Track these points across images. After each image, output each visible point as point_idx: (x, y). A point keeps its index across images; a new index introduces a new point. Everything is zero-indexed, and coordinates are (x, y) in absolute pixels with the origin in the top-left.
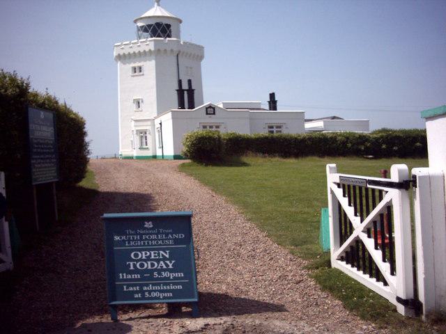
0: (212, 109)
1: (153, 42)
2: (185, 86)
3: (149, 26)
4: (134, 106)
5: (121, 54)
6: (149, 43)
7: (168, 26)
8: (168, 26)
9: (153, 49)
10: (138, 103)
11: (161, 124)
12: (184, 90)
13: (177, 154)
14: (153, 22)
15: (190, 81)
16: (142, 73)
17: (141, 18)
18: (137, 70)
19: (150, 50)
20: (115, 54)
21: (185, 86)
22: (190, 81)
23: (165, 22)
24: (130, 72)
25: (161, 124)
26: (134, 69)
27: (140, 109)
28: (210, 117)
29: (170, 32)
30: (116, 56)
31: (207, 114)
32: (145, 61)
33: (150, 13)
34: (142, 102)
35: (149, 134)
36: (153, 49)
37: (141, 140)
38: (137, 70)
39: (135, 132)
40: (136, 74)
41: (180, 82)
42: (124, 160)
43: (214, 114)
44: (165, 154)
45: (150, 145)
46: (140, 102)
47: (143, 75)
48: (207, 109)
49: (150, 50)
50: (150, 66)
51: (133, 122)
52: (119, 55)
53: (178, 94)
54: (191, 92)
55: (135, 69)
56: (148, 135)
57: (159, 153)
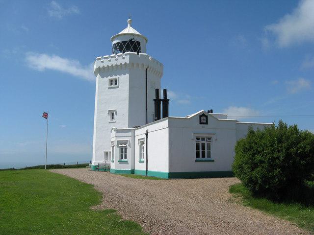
0: (205, 118)
1: (128, 56)
2: (162, 97)
3: (124, 42)
4: (109, 117)
5: (101, 67)
6: (124, 58)
7: (139, 43)
8: (139, 43)
9: (128, 62)
10: (112, 114)
11: (147, 134)
12: (161, 100)
13: (173, 171)
14: (127, 39)
15: (165, 91)
16: (117, 85)
17: (118, 36)
18: (114, 83)
19: (126, 63)
20: (95, 67)
21: (162, 97)
22: (165, 91)
23: (137, 39)
24: (108, 85)
25: (147, 134)
26: (111, 82)
27: (114, 121)
28: (203, 127)
29: (140, 49)
30: (97, 69)
31: (201, 123)
32: (120, 75)
33: (125, 31)
34: (116, 113)
35: (129, 145)
36: (128, 62)
37: (122, 152)
38: (114, 83)
39: (115, 144)
40: (113, 86)
41: (157, 91)
42: (96, 173)
43: (207, 123)
44: (148, 170)
45: (129, 159)
46: (114, 113)
47: (118, 87)
48: (201, 116)
49: (126, 63)
50: (124, 80)
51: (114, 133)
52: (99, 67)
53: (155, 104)
54: (166, 101)
55: (112, 81)
56: (195, 158)
57: (140, 167)
